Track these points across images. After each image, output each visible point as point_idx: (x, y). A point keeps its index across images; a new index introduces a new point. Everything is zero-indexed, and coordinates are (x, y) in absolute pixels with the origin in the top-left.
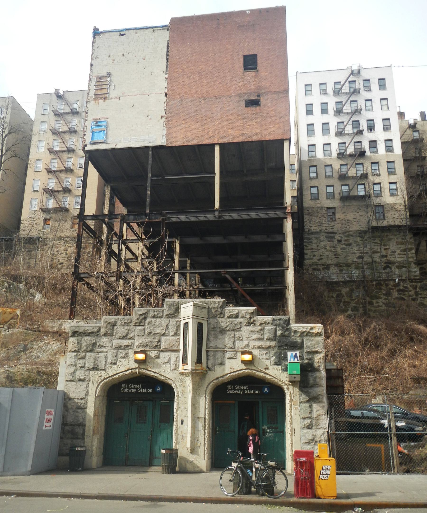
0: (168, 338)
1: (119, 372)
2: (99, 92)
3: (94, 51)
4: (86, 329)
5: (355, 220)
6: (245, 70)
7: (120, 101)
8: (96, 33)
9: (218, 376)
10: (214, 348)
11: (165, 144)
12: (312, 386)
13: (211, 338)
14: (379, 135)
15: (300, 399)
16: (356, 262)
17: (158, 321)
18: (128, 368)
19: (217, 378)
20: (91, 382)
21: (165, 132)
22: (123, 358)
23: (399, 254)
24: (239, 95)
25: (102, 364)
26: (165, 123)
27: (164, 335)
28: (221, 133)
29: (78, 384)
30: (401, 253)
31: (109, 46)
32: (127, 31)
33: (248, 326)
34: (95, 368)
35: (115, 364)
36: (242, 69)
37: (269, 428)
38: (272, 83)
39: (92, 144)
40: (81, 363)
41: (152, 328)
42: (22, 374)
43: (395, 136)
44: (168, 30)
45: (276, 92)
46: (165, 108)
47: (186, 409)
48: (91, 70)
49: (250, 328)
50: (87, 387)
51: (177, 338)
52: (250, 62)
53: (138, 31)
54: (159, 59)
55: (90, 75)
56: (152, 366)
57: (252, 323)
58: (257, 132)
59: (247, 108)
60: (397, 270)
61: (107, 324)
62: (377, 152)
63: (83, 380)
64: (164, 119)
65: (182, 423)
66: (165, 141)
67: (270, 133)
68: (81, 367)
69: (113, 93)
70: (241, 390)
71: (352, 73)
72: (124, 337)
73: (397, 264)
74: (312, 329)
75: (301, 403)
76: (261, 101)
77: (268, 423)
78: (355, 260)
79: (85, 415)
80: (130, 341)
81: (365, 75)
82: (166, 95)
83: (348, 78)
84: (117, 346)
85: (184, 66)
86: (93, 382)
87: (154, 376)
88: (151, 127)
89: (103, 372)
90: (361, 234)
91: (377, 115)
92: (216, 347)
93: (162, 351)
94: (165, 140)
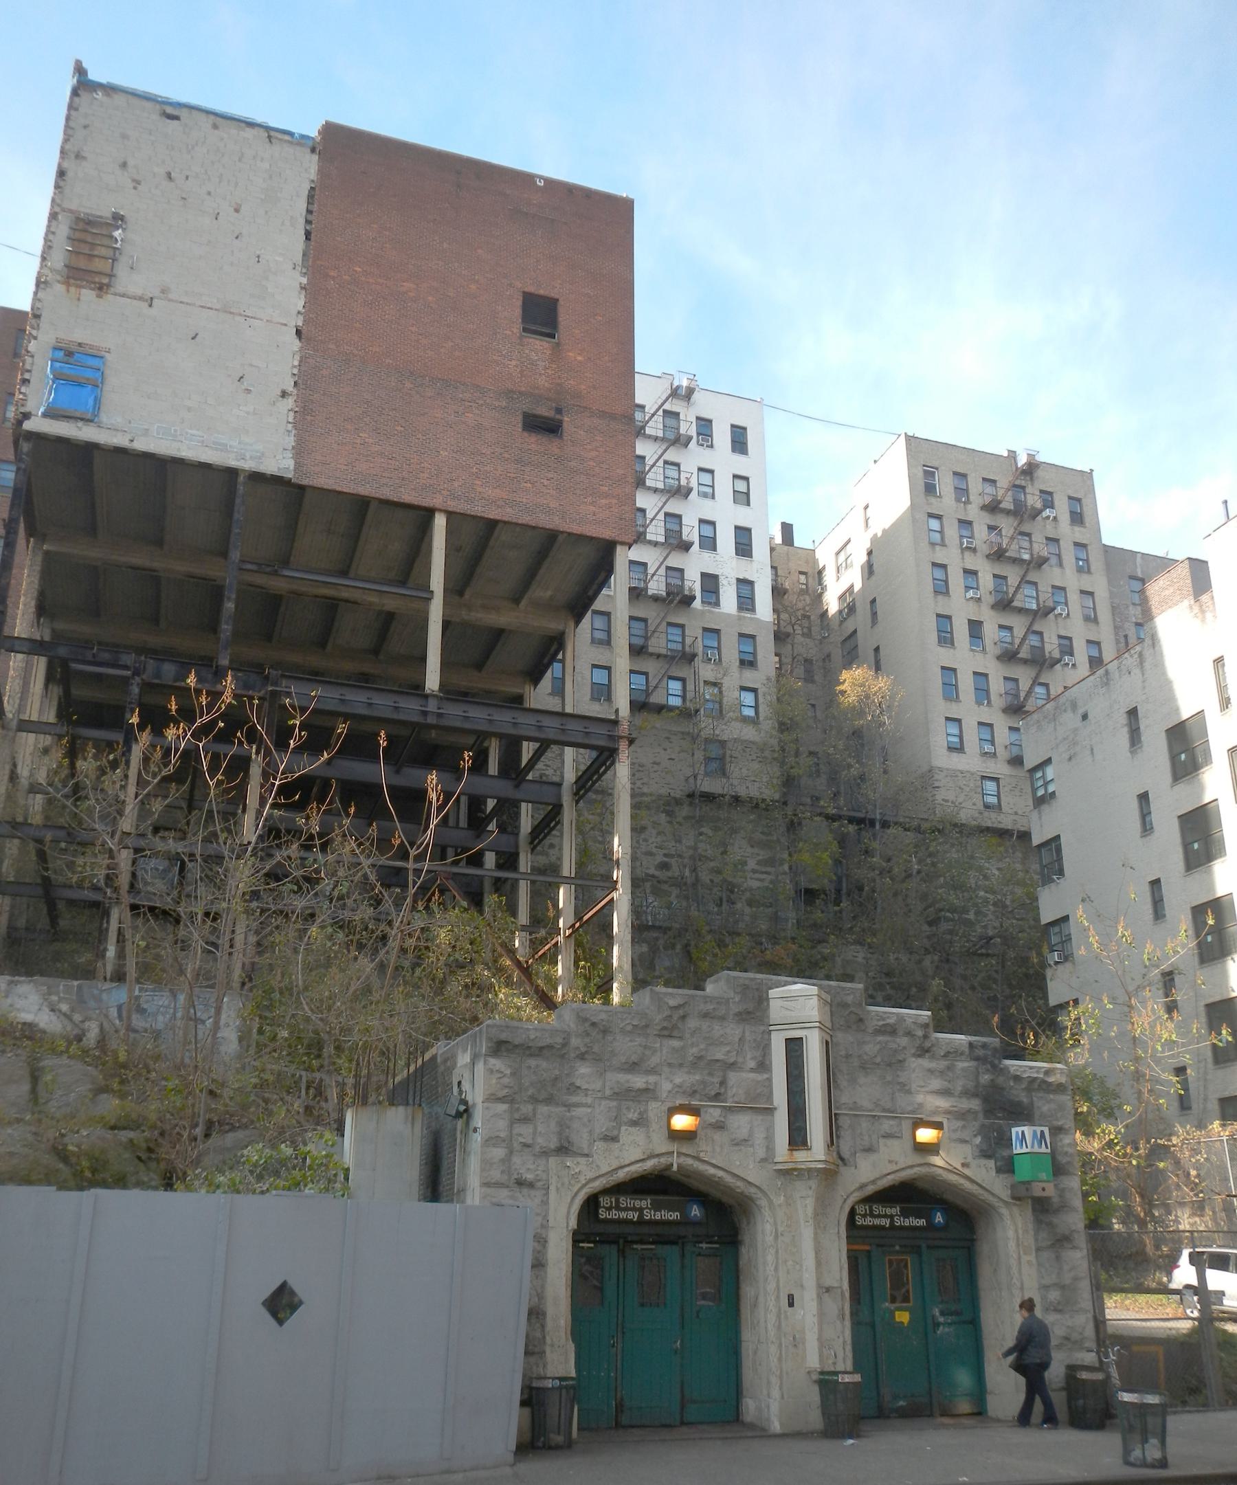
0: (744, 1075)
1: (627, 1162)
2: (83, 263)
3: (70, 132)
4: (532, 1037)
5: (656, 767)
6: (525, 330)
7: (153, 312)
8: (83, 85)
9: (864, 1180)
10: (851, 1109)
11: (290, 476)
12: (1057, 1211)
13: (843, 1081)
14: (726, 564)
15: (1036, 1240)
16: (653, 876)
17: (717, 1030)
18: (648, 1153)
19: (862, 1187)
20: (552, 1188)
21: (290, 441)
22: (634, 1123)
23: (754, 871)
24: (509, 394)
25: (581, 1139)
26: (292, 414)
27: (732, 1066)
28: (456, 484)
29: (518, 1194)
30: (757, 867)
31: (124, 137)
32: (185, 110)
33: (919, 1056)
34: (564, 1149)
35: (615, 1139)
36: (517, 327)
37: (942, 1313)
38: (594, 387)
39: (50, 414)
40: (525, 1131)
41: (702, 1046)
42: (11, 1154)
43: (760, 573)
44: (313, 150)
45: (603, 415)
46: (295, 371)
47: (798, 1267)
48: (57, 186)
49: (925, 1063)
50: (545, 1203)
51: (766, 1076)
52: (541, 315)
53: (219, 121)
54: (283, 224)
55: (53, 200)
56: (709, 1149)
57: (927, 1051)
58: (552, 505)
59: (526, 434)
60: (747, 910)
61: (587, 1025)
62: (717, 604)
63: (531, 1185)
64: (290, 402)
65: (791, 1304)
66: (292, 468)
67: (587, 518)
68: (526, 1145)
69: (127, 280)
70: (885, 1216)
71: (674, 393)
72: (633, 1067)
73: (748, 894)
74: (1048, 1072)
75: (1038, 1250)
76: (565, 425)
77: (942, 1302)
78: (652, 871)
79: (543, 1287)
80: (652, 1079)
81: (703, 406)
82: (299, 333)
83: (665, 402)
84: (617, 1090)
85: (358, 269)
86: (558, 1189)
87: (714, 1176)
88: (248, 413)
89: (583, 1160)
90: (669, 805)
91: (727, 516)
92: (855, 1106)
93: (730, 1109)
94: (290, 464)
